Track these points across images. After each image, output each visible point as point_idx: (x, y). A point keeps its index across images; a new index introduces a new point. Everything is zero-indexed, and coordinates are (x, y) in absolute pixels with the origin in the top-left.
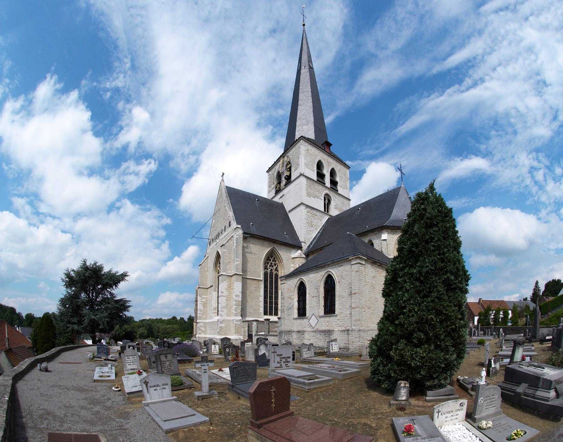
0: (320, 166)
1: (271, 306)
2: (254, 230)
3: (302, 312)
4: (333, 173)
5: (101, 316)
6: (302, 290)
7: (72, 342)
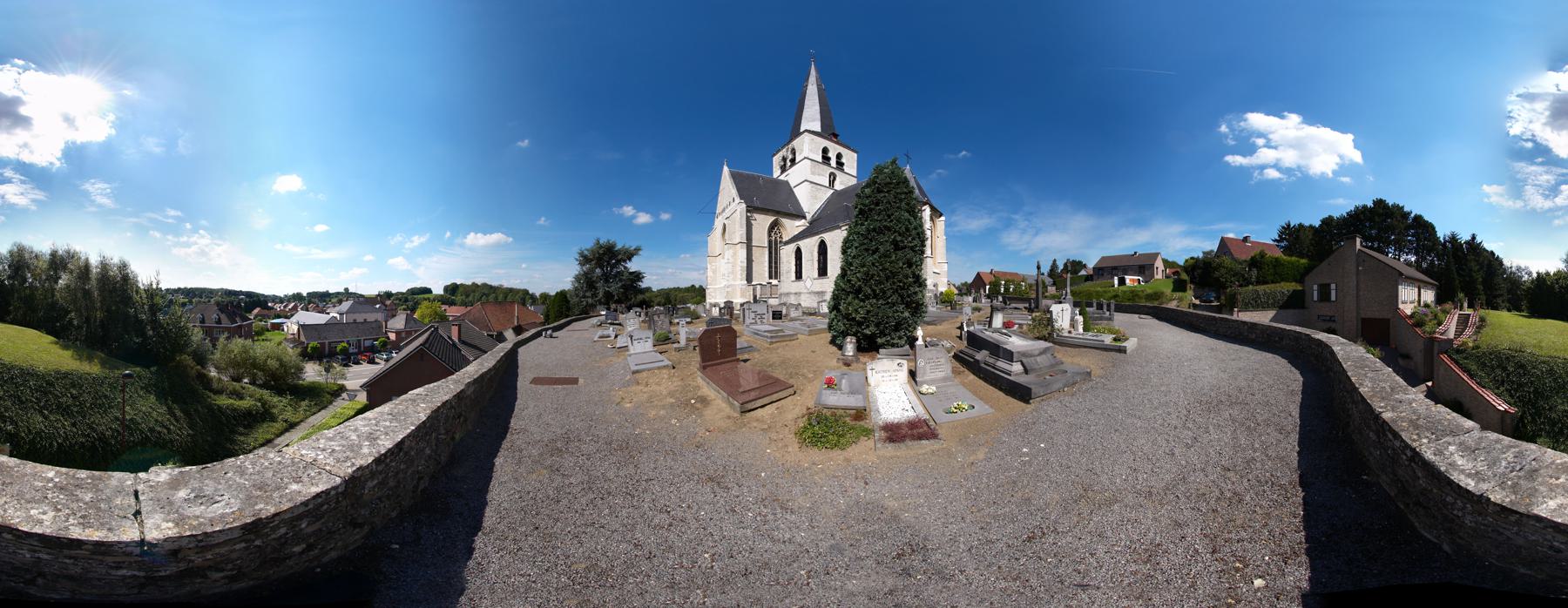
0: (825, 151)
1: (774, 271)
2: (757, 204)
3: (799, 275)
4: (839, 156)
5: (615, 287)
6: (798, 253)
7: (586, 313)
